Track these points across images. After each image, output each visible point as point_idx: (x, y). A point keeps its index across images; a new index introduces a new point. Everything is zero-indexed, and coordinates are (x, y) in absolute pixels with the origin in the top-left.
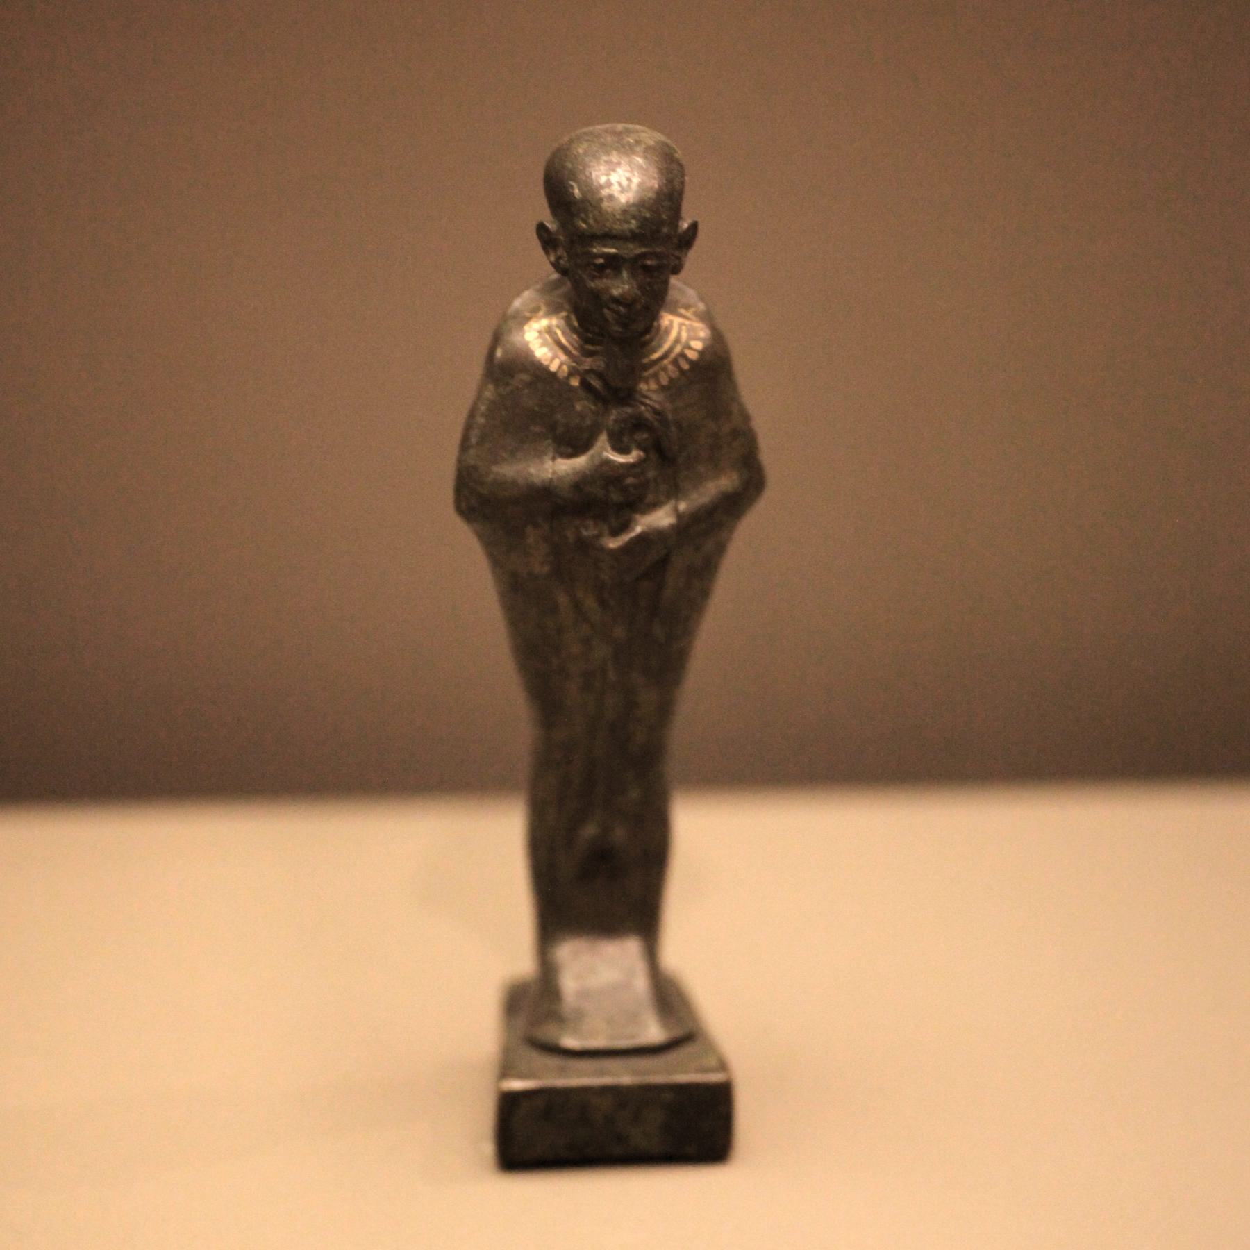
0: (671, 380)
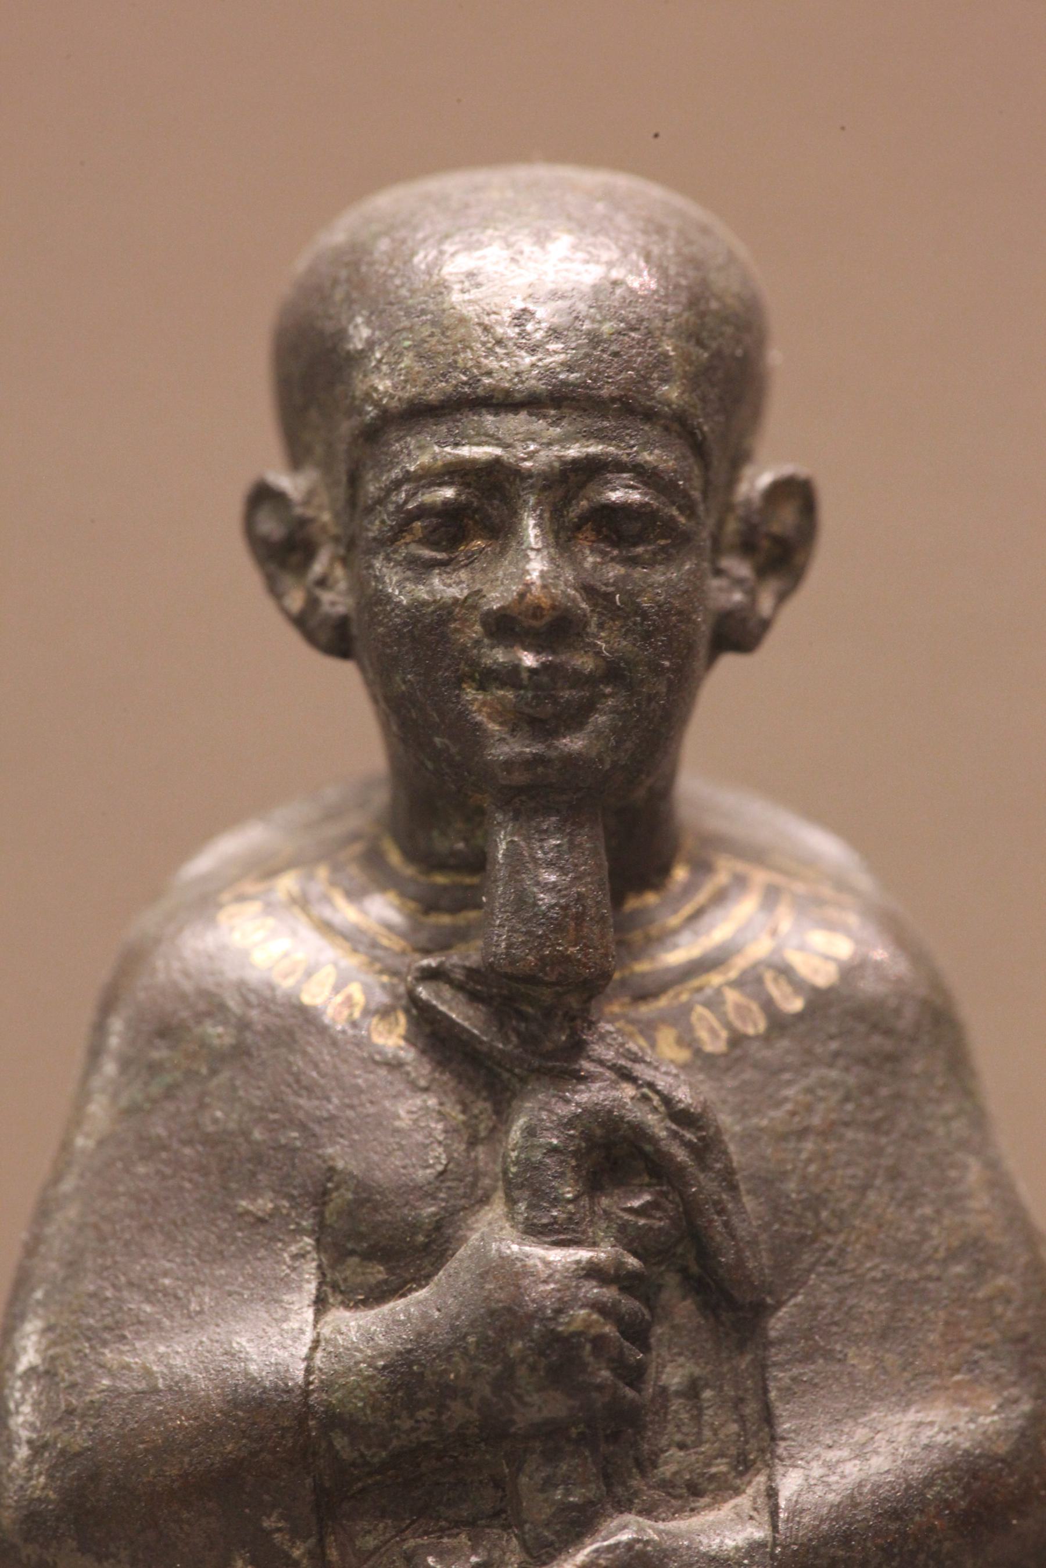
0: (737, 1040)
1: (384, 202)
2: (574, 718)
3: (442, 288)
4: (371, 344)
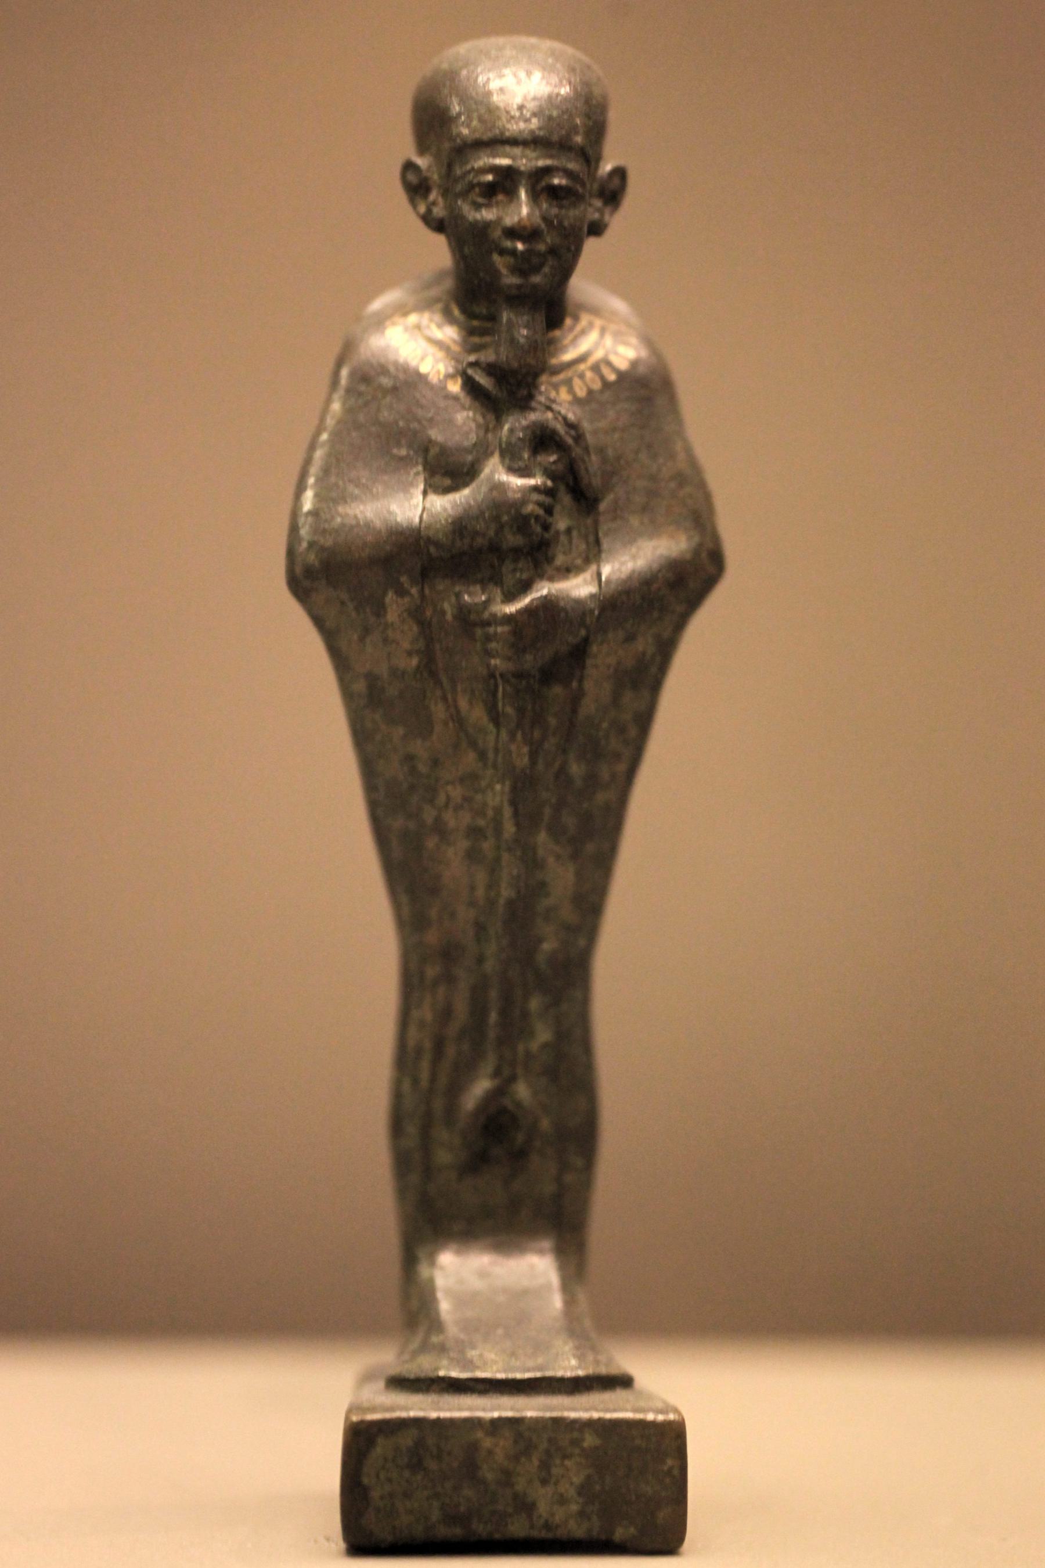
0: (590, 392)
1: (463, 49)
2: (537, 269)
3: (489, 94)
4: (459, 115)
